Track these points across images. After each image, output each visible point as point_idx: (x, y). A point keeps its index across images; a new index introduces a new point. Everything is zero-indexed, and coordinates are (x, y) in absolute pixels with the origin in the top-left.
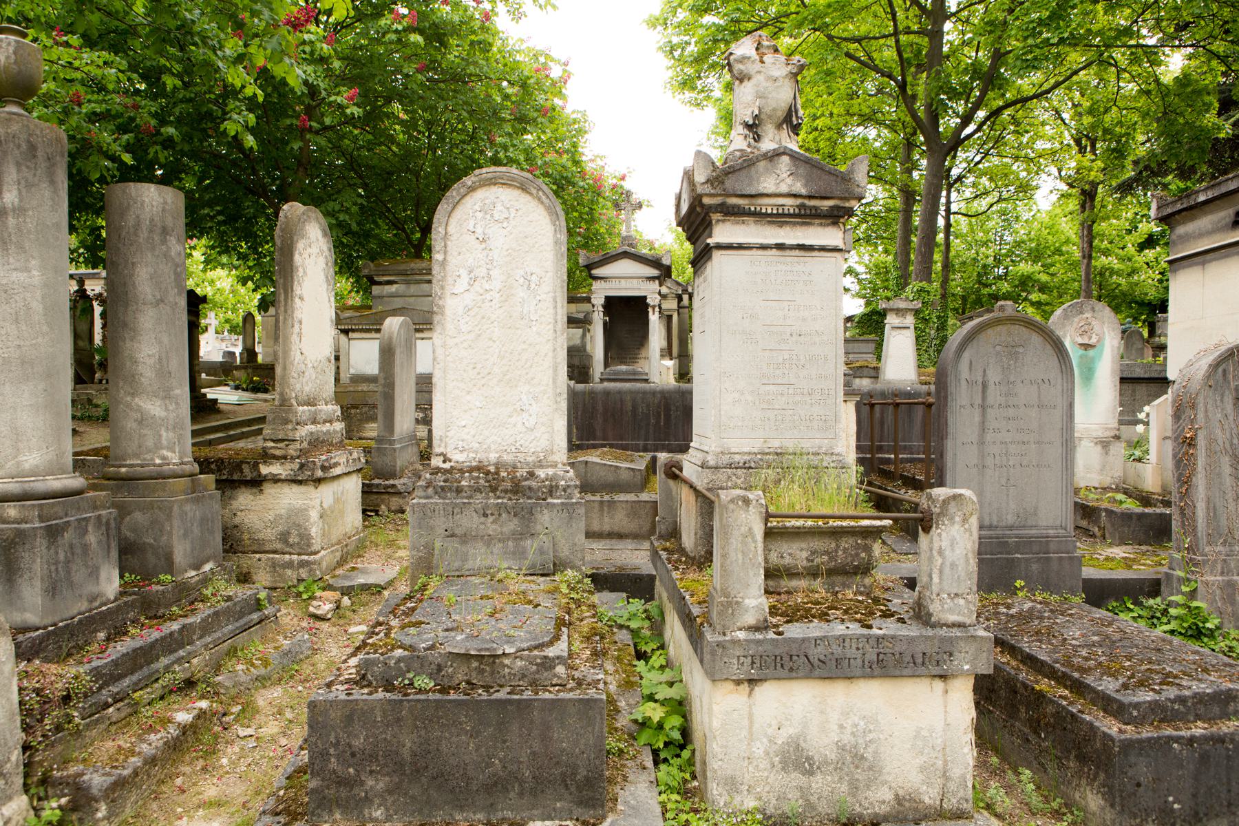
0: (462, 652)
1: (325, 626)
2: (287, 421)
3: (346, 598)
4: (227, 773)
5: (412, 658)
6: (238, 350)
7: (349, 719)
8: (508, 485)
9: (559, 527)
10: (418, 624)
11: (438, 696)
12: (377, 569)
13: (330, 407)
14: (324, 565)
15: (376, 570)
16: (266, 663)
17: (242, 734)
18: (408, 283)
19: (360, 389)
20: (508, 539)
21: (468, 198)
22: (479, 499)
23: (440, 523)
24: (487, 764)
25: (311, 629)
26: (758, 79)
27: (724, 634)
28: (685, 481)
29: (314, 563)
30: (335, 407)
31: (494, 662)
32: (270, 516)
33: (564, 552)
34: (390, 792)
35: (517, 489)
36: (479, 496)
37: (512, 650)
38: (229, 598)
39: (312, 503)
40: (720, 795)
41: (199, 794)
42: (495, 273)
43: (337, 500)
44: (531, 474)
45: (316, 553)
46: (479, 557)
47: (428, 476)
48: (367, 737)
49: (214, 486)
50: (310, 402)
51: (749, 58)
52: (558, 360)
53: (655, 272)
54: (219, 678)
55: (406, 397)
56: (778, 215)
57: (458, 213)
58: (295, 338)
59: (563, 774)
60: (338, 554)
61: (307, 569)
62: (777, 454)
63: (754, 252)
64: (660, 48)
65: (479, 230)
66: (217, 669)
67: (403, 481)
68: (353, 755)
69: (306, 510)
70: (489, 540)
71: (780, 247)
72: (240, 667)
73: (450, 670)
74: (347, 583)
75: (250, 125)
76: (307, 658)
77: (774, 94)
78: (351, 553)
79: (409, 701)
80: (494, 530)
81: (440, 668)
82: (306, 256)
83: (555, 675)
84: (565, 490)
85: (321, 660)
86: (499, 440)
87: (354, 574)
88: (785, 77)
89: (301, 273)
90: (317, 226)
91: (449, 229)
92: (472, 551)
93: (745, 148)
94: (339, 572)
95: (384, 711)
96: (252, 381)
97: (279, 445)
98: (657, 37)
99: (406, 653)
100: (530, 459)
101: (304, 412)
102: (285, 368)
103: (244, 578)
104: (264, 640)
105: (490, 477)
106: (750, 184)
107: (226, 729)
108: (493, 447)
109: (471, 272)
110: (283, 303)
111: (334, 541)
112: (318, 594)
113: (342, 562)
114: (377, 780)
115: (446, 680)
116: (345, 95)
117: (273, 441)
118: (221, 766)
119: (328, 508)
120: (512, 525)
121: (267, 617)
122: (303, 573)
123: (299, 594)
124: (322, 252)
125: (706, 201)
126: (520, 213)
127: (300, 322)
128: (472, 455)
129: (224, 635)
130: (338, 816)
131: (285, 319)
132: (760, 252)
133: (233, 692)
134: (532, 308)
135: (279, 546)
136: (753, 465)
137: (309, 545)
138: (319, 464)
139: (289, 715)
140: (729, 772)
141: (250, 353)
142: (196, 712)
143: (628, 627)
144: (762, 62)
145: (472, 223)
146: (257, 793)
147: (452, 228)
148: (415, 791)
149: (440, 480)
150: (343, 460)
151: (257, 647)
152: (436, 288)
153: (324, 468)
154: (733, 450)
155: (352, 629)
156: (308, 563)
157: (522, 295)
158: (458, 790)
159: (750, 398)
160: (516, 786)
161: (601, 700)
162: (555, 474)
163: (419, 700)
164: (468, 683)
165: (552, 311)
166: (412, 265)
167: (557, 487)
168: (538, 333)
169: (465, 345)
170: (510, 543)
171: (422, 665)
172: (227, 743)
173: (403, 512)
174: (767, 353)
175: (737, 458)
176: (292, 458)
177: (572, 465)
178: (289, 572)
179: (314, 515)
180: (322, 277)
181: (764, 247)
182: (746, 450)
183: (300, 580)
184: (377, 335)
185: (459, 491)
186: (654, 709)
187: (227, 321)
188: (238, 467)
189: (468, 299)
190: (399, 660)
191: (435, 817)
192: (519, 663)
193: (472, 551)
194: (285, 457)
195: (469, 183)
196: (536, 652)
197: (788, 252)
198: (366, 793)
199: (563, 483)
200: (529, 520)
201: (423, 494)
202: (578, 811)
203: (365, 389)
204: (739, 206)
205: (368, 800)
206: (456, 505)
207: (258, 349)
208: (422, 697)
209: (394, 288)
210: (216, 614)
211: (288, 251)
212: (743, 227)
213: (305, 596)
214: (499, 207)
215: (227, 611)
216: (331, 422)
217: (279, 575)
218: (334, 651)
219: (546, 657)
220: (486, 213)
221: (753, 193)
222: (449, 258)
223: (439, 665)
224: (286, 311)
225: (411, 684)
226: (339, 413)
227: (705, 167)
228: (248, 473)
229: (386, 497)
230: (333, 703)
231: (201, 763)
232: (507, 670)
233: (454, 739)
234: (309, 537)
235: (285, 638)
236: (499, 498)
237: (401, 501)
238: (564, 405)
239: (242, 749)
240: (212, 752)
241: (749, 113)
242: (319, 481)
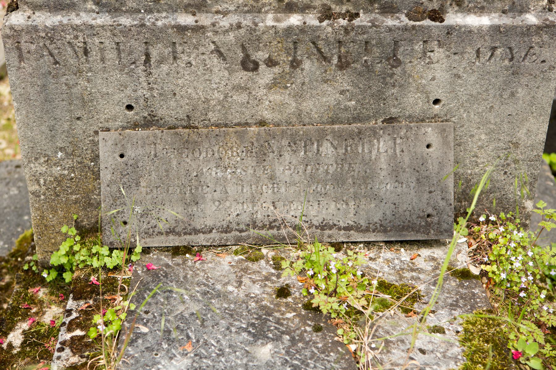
9: (473, 99)
20: (321, 136)
23: (111, 91)
46: (232, 190)
70: (264, 139)
92: (212, 173)
120: (326, 93)
170: (327, 149)
193: (212, 173)
200: (384, 77)
206: (157, 34)
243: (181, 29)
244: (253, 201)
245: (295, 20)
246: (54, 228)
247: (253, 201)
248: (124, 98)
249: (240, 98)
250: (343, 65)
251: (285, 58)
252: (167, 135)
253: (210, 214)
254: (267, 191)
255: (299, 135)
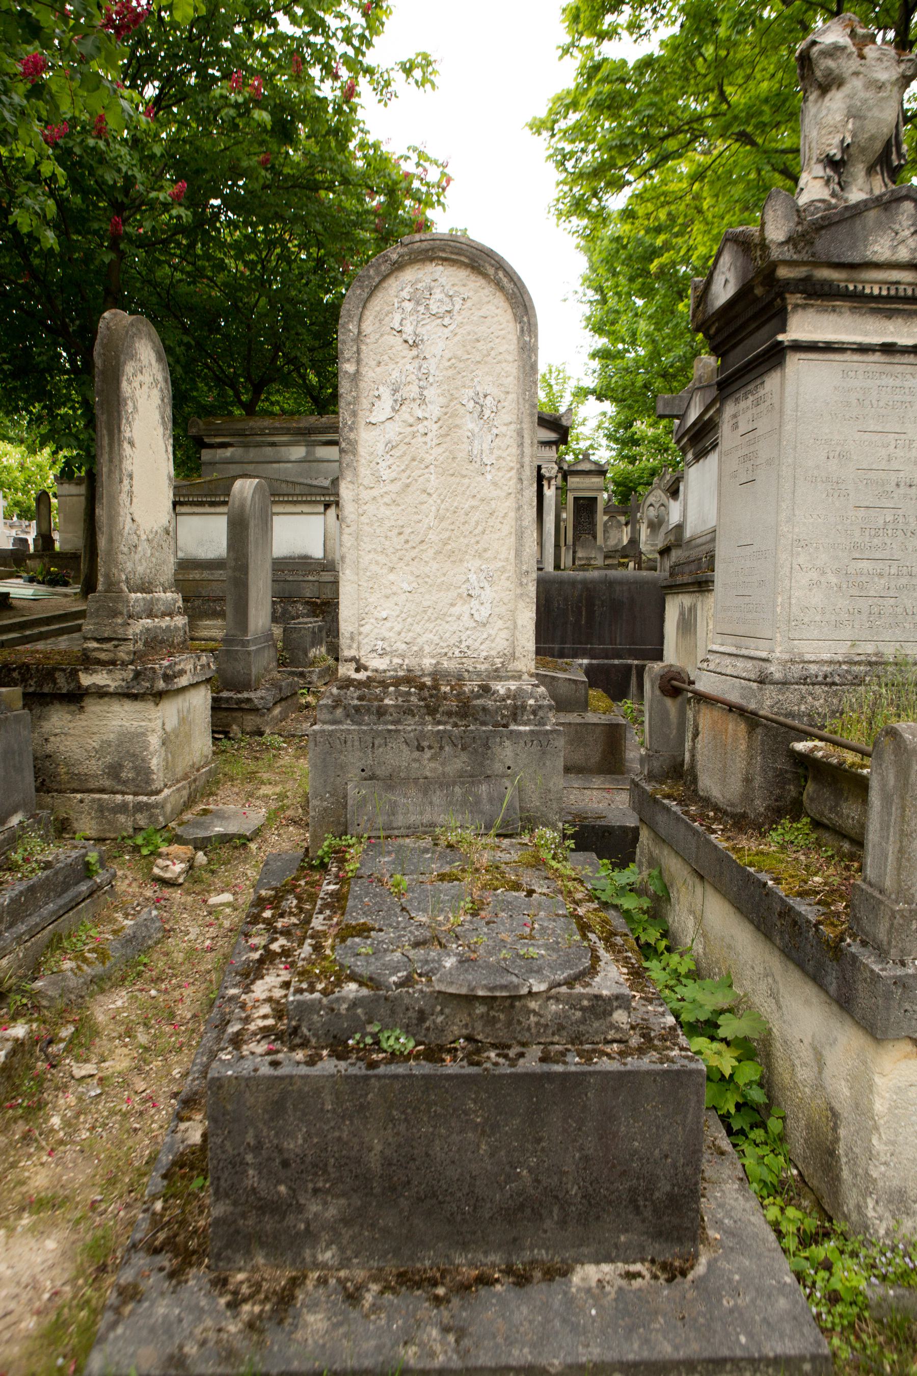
0: (464, 991)
1: (177, 895)
2: (115, 613)
3: (200, 853)
4: (61, 1142)
5: (376, 1000)
6: (31, 538)
7: (278, 1108)
8: (453, 704)
10: (363, 931)
11: (425, 1068)
12: (236, 814)
13: (169, 595)
14: (168, 808)
15: (235, 814)
16: (103, 956)
17: (79, 1072)
18: (246, 446)
19: (191, 577)
21: (391, 281)
22: (410, 726)
23: (354, 759)
24: (508, 1176)
25: (158, 900)
26: (856, 84)
27: (903, 964)
28: (702, 698)
29: (155, 806)
30: (175, 596)
31: (512, 1006)
32: (94, 743)
33: (534, 801)
34: (346, 1222)
35: (465, 710)
36: (410, 720)
37: (543, 987)
38: (48, 865)
39: (152, 725)
40: (880, 1219)
41: (22, 1183)
42: (430, 393)
43: (183, 720)
44: (486, 689)
45: (158, 792)
46: (411, 808)
47: (335, 691)
48: (309, 1135)
49: (20, 704)
50: (145, 587)
51: (844, 48)
52: (525, 523)
53: (552, 436)
54: (39, 984)
55: (261, 584)
56: (889, 299)
57: (377, 304)
58: (124, 498)
59: (633, 1190)
60: (185, 793)
61: (146, 814)
62: (870, 664)
63: (848, 356)
64: (550, 156)
65: (408, 329)
66: (35, 970)
67: (259, 693)
68: (285, 1164)
69: (143, 734)
70: (426, 785)
71: (888, 349)
72: (68, 965)
73: (440, 1019)
74: (201, 834)
75: (49, 217)
76: (156, 943)
77: (876, 113)
78: (201, 788)
79: (379, 1077)
80: (433, 770)
81: (422, 1016)
82: (136, 384)
83: (612, 1026)
84: (534, 713)
85: (177, 947)
86: (436, 639)
87: (207, 819)
88: (893, 84)
89: (130, 407)
90: (150, 346)
91: (364, 326)
93: (828, 197)
94: (187, 816)
95: (337, 1094)
96: (49, 573)
97: (104, 646)
98: (542, 144)
99: (365, 991)
100: (482, 667)
101: (137, 600)
102: (111, 540)
103: (63, 828)
104: (98, 920)
105: (426, 693)
106: (853, 247)
107: (54, 1067)
108: (427, 649)
109: (395, 391)
110: (107, 449)
111: (179, 775)
112: (164, 849)
113: (189, 803)
114: (325, 1203)
115: (432, 1036)
116: (170, 191)
117: (98, 640)
118: (52, 1130)
119: (171, 729)
120: (458, 763)
121: (100, 887)
122: (142, 819)
123: (137, 849)
124: (156, 382)
125: (783, 272)
126: (469, 303)
127: (131, 476)
128: (397, 661)
129: (43, 919)
130: (260, 1260)
131: (110, 471)
132: (857, 357)
133: (60, 1004)
134: (486, 446)
135: (107, 783)
136: (837, 679)
137: (148, 781)
138: (160, 672)
139: (143, 1038)
140: (896, 1183)
141: (45, 539)
142: (9, 1045)
143: (616, 907)
144: (862, 57)
145: (397, 317)
146: (112, 1181)
147: (368, 326)
148: (388, 1220)
149: (352, 697)
150: (189, 667)
151: (95, 934)
152: (344, 414)
153: (167, 678)
154: (808, 657)
155: (214, 900)
156: (147, 807)
157: (471, 426)
158: (459, 1218)
159: (834, 580)
160: (556, 1210)
161: (699, 1072)
162: (520, 689)
163: (396, 1077)
164: (469, 1039)
165: (514, 450)
166: (251, 424)
167: (524, 707)
168: (495, 484)
169: (387, 499)
170: (457, 789)
171: (393, 1012)
172: (57, 1089)
173: (261, 734)
174: (862, 513)
175: (813, 669)
176: (124, 664)
177: (542, 679)
178: (122, 818)
179: (154, 741)
180: (157, 416)
181: (863, 349)
182: (826, 656)
183: (138, 829)
184: (224, 509)
185: (381, 712)
186: (719, 1053)
187: (17, 504)
188: (49, 675)
189: (392, 431)
190: (355, 1004)
191: (422, 1260)
192: (553, 1007)
194: (113, 663)
195: (394, 257)
196: (579, 989)
197: (898, 358)
198: (308, 1225)
199: (531, 702)
200: (484, 755)
201: (328, 717)
202: (654, 1248)
203: (197, 577)
204: (829, 283)
205: (310, 1236)
206: (378, 733)
207: (56, 536)
208: (400, 1069)
209: (228, 452)
210: (31, 889)
211: (114, 376)
212: (833, 317)
213: (145, 852)
214: (438, 294)
215: (45, 885)
216: (171, 615)
217: (110, 823)
218: (194, 931)
219: (598, 997)
220: (418, 303)
221: (857, 260)
222: (364, 370)
223: (421, 1012)
224: (111, 461)
225: (377, 1042)
226: (180, 603)
227: (786, 217)
228: (63, 684)
229: (239, 714)
230: (251, 1082)
231: (20, 1128)
232: (533, 1019)
233: (455, 1137)
234: (148, 772)
235: (126, 916)
236: (439, 723)
237: (258, 720)
238: (532, 589)
239: (80, 1099)
240: (36, 1109)
241: (836, 141)
242: (159, 696)
243: (389, 731)
244: (421, 814)
245: (441, 727)
246: (63, 1307)
247: (421, 814)
248: (360, 765)
249: (415, 765)
250: (463, 749)
251: (436, 745)
252: (380, 783)
253: (400, 820)
254: (428, 809)
255: (444, 783)
